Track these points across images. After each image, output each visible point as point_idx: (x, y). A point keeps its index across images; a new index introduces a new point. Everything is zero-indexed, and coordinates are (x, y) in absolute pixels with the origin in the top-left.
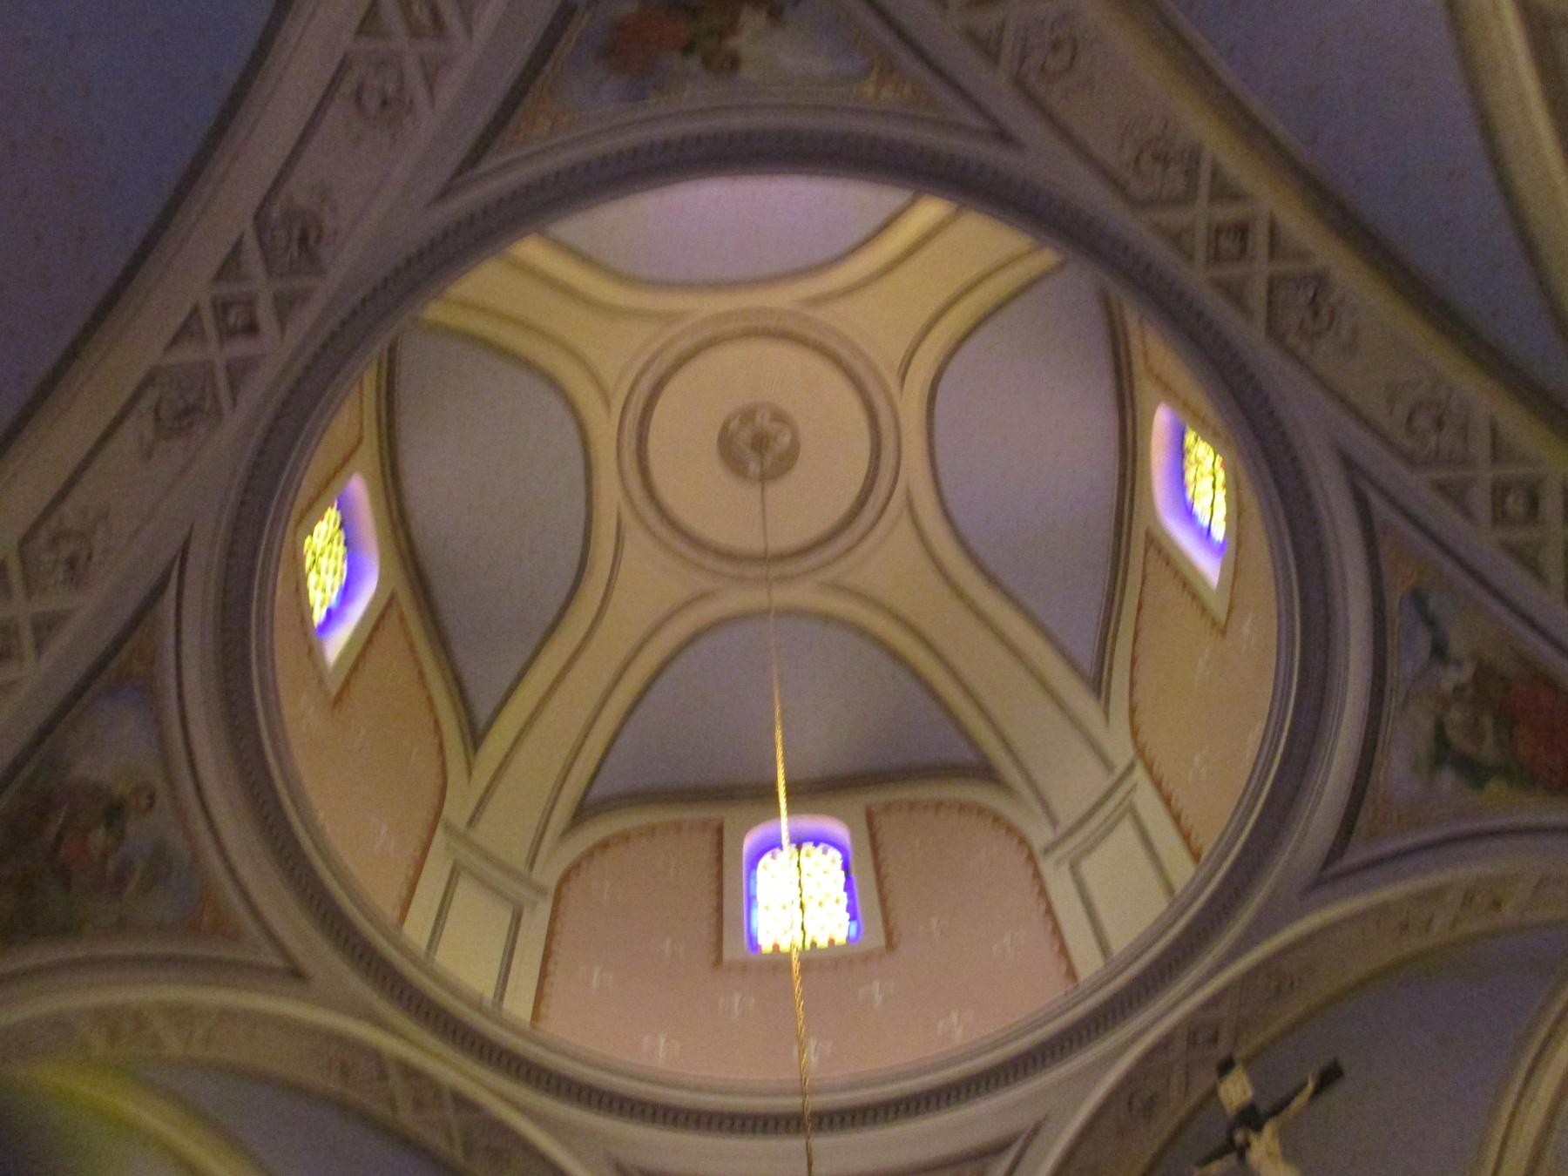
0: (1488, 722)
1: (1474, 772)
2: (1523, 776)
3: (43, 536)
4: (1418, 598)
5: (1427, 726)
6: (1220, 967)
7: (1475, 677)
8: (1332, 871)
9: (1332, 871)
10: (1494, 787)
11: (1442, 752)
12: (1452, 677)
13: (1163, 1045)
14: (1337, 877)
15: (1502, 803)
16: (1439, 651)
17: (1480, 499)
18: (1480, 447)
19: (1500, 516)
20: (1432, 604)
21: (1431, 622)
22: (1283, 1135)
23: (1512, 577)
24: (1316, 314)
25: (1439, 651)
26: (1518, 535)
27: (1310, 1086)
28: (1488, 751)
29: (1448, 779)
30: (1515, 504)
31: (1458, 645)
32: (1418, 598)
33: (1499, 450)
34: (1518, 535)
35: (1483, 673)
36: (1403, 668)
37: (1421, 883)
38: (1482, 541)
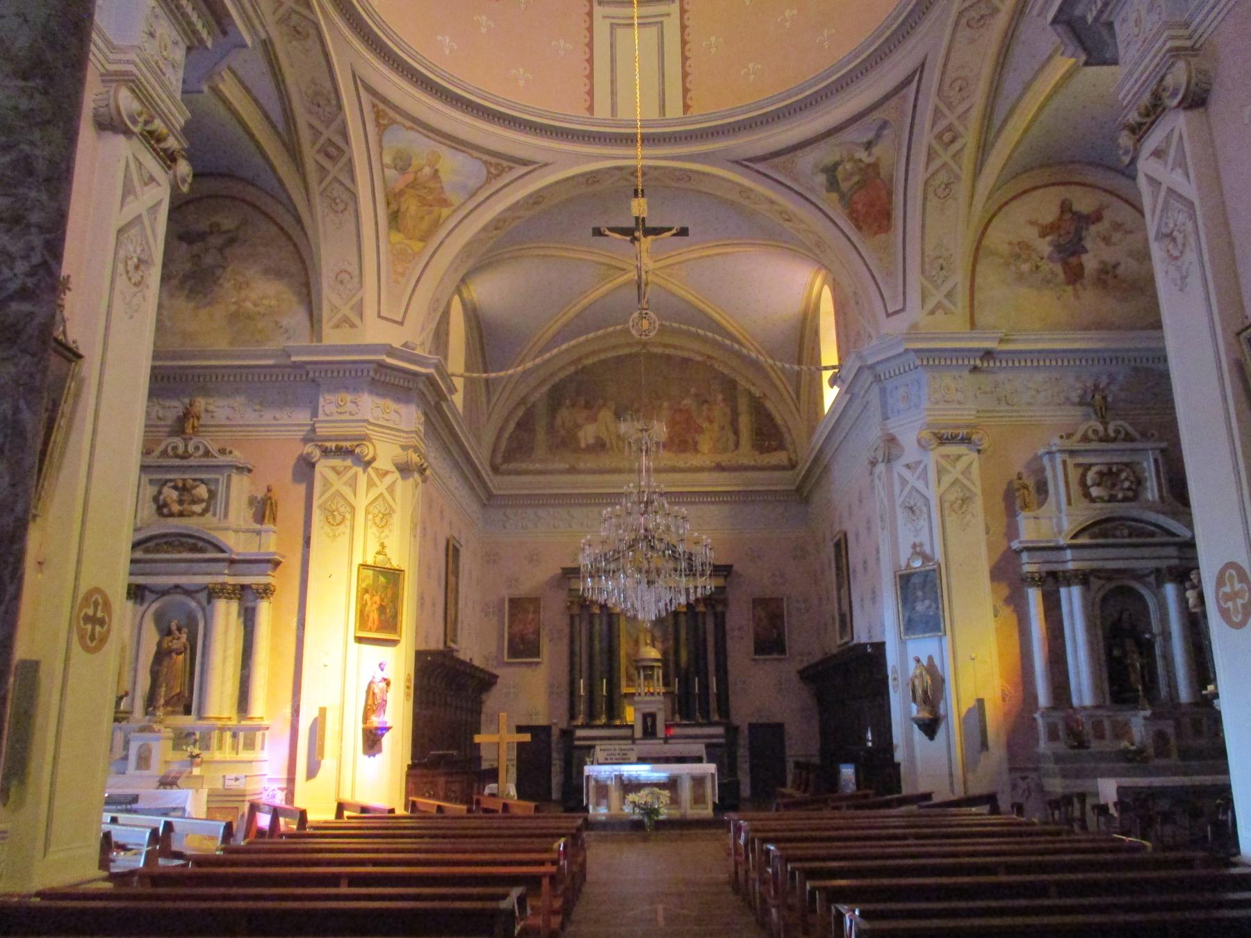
0: (856, 179)
1: (833, 185)
2: (846, 201)
3: (927, 267)
4: (884, 125)
5: (837, 158)
6: (673, 158)
7: (869, 165)
8: (745, 163)
9: (745, 163)
10: (834, 196)
11: (831, 171)
12: (862, 155)
13: (620, 168)
14: (747, 167)
15: (830, 202)
16: (869, 145)
17: (942, 124)
18: (960, 109)
19: (939, 137)
20: (886, 132)
21: (878, 136)
22: (653, 241)
23: (920, 156)
24: (979, 21)
25: (869, 145)
26: (937, 147)
27: (674, 231)
28: (845, 186)
29: (821, 179)
30: (947, 137)
31: (877, 151)
32: (884, 125)
33: (963, 117)
34: (937, 147)
35: (875, 166)
36: (850, 135)
37: (770, 193)
38: (925, 137)
